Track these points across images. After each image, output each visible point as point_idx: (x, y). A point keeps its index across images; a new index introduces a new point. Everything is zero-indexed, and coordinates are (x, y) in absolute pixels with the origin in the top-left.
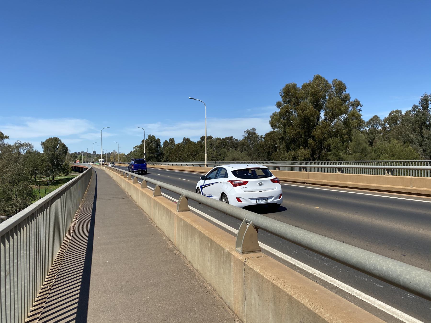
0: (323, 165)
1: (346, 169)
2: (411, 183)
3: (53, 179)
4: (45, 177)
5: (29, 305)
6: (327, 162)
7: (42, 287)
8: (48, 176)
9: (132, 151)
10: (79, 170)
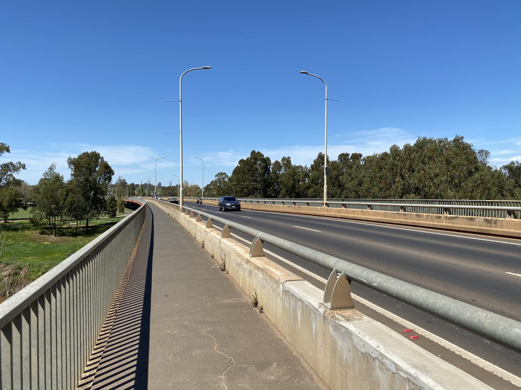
0: (425, 204)
1: (465, 210)
3: (87, 223)
4: (74, 219)
6: (427, 201)
8: (77, 218)
9: (213, 181)
10: (133, 206)
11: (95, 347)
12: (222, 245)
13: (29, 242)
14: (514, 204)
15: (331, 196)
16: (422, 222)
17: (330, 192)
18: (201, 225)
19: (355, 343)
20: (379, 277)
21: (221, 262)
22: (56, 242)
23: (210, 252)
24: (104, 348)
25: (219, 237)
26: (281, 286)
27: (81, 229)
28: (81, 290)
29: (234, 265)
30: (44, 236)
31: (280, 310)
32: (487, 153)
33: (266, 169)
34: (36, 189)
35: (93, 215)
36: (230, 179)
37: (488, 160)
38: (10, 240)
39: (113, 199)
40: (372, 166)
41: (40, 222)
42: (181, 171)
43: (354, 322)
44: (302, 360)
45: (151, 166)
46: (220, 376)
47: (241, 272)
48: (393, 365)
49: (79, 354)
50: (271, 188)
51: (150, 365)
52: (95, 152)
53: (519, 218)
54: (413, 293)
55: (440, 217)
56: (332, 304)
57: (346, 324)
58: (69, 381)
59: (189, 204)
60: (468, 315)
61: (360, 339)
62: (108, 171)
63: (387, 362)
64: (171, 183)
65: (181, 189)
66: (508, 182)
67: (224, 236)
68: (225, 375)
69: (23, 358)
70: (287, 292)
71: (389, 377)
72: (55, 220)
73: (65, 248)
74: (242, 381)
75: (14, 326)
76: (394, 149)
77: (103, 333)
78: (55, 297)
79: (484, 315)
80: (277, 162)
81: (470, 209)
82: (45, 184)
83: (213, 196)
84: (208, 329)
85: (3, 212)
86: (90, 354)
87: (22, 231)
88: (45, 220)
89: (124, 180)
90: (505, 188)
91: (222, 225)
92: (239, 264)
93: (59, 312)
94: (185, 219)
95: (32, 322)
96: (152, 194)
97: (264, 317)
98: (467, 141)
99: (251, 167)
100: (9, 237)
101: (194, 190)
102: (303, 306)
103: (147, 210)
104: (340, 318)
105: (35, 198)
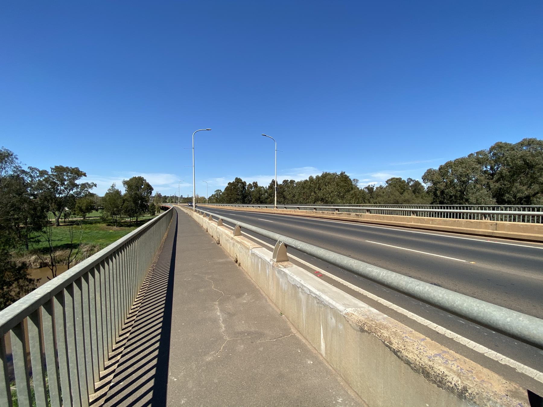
2: (453, 224)
5: (105, 348)
7: (130, 311)
11: (140, 291)
12: (218, 230)
13: (100, 231)
14: (370, 206)
15: (279, 203)
16: (325, 216)
17: (278, 200)
18: (205, 219)
19: (289, 279)
20: (301, 244)
21: (217, 239)
22: (117, 230)
23: (211, 234)
24: (145, 291)
25: (216, 226)
26: (250, 251)
27: (133, 223)
28: (130, 257)
29: (225, 241)
30: (110, 227)
31: (250, 264)
32: (357, 181)
33: (244, 188)
34: (103, 199)
35: (140, 214)
36: (223, 193)
37: (358, 184)
38: (87, 230)
39: (153, 205)
40: (299, 187)
41: (107, 218)
42: (194, 188)
43: (288, 268)
44: (261, 291)
45: (176, 186)
46: (215, 303)
47: (228, 245)
48: (308, 290)
49: (129, 295)
50: (247, 199)
51: (174, 299)
52: (140, 177)
53: (526, 221)
54: (318, 252)
55: (333, 213)
56: (277, 260)
57: (284, 270)
58: (123, 311)
59: (200, 208)
60: (346, 262)
61: (292, 278)
62: (149, 188)
63: (305, 289)
64: (188, 196)
65: (194, 199)
66: (367, 196)
67: (219, 225)
68: (218, 302)
69: (90, 299)
70: (253, 254)
71: (306, 297)
72: (116, 218)
73: (123, 234)
74: (228, 304)
75: (83, 280)
76: (311, 178)
77: (145, 282)
78: (112, 261)
79: (353, 262)
80: (250, 184)
81: (385, 210)
82: (110, 196)
83: (213, 203)
84: (209, 277)
85: (83, 213)
86: (137, 295)
87: (95, 224)
88: (110, 218)
89: (160, 194)
90: (366, 198)
91: (217, 219)
92: (227, 240)
93: (115, 270)
94: (196, 216)
95: (96, 277)
96: (177, 202)
97: (241, 268)
98: (347, 174)
99: (235, 186)
100: (86, 228)
101: (202, 199)
102: (262, 261)
103: (174, 211)
104: (281, 266)
105: (103, 204)
